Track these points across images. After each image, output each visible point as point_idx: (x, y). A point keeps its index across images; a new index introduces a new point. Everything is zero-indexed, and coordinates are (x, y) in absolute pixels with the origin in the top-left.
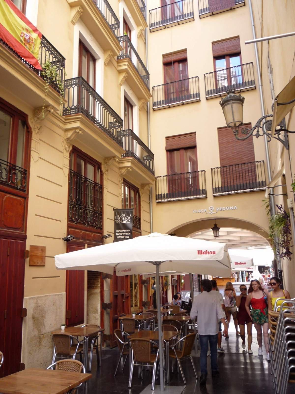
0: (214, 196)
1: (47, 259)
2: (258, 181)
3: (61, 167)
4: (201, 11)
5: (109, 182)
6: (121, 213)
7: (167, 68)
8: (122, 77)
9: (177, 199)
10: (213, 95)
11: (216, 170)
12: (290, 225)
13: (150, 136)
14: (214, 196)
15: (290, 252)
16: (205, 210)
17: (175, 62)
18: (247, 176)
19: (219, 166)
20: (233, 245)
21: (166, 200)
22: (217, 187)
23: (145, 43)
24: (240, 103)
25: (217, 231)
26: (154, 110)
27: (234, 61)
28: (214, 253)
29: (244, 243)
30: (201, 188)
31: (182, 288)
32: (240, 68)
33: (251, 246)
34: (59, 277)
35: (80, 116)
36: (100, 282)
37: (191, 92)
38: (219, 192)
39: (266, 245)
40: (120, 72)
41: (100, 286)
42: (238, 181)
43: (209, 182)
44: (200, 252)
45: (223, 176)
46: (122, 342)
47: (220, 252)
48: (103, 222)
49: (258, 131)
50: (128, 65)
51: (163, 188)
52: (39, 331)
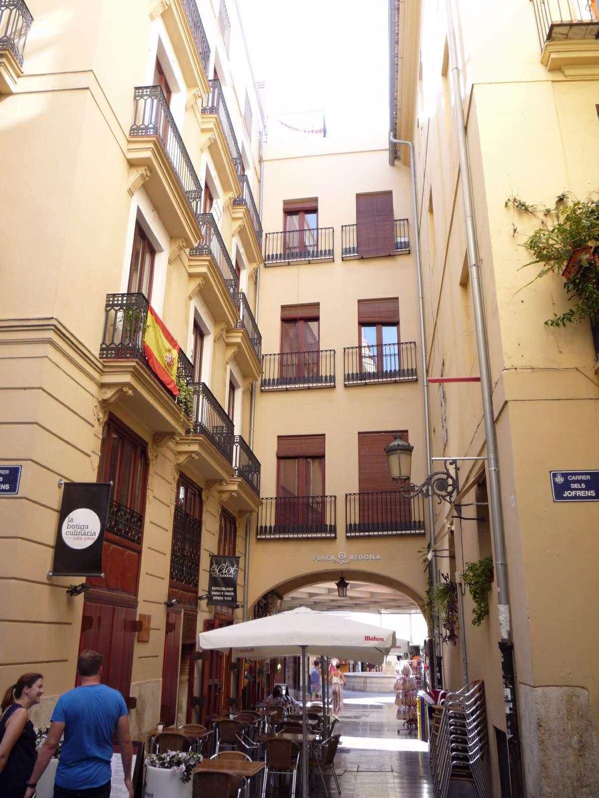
0: (347, 537)
1: (152, 632)
2: (413, 520)
3: (168, 504)
4: (346, 251)
5: (208, 513)
6: (220, 560)
7: (286, 325)
8: (231, 352)
9: (291, 536)
10: (354, 382)
11: (352, 497)
12: (457, 601)
13: (253, 431)
14: (347, 537)
15: (454, 635)
16: (333, 557)
17: (299, 318)
18: (398, 510)
19: (357, 491)
20: (356, 604)
21: (272, 536)
22: (353, 523)
23: (256, 284)
24: (407, 454)
25: (345, 588)
26: (262, 391)
27: (389, 334)
28: (382, 640)
29: (375, 602)
30: (328, 523)
31: (278, 678)
32: (396, 347)
33: (386, 608)
34: (158, 656)
35: (201, 438)
36: (188, 665)
37: (323, 373)
38: (355, 531)
39: (413, 609)
40: (228, 345)
41: (187, 670)
42: (384, 516)
43: (341, 514)
44: (367, 638)
45: (363, 507)
46: (247, 747)
47: (388, 639)
48: (198, 575)
49: (427, 490)
50: (242, 339)
51: (268, 516)
52: (140, 729)
